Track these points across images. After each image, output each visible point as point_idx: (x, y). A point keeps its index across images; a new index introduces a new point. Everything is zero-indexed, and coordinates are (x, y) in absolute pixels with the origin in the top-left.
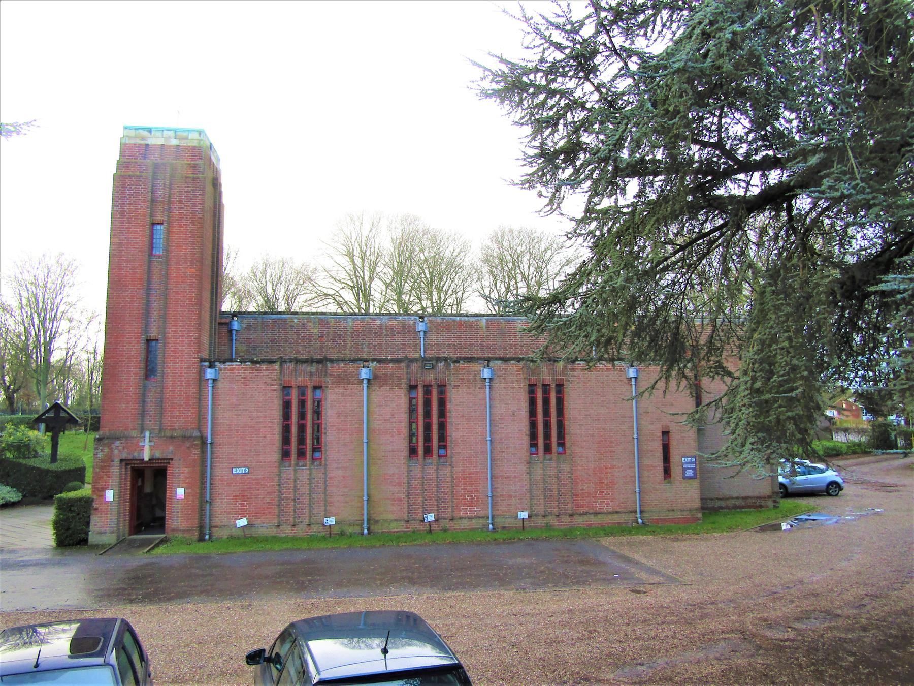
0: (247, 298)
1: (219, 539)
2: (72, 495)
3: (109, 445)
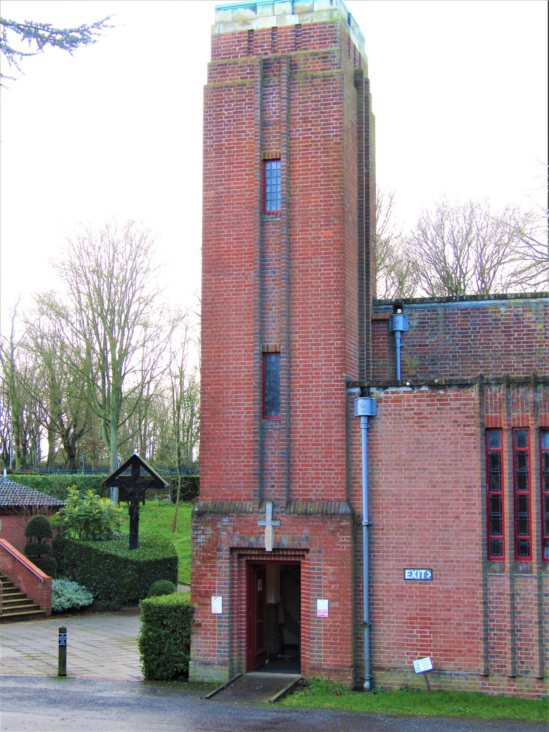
0: (412, 274)
1: (386, 690)
2: (163, 600)
3: (213, 523)
